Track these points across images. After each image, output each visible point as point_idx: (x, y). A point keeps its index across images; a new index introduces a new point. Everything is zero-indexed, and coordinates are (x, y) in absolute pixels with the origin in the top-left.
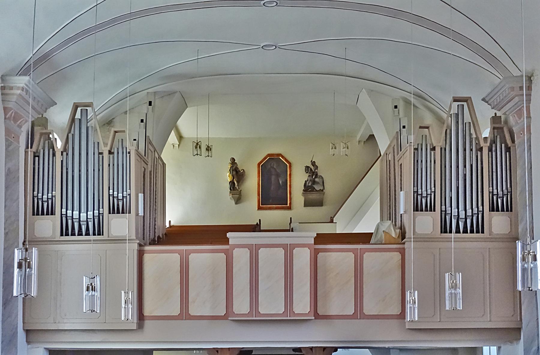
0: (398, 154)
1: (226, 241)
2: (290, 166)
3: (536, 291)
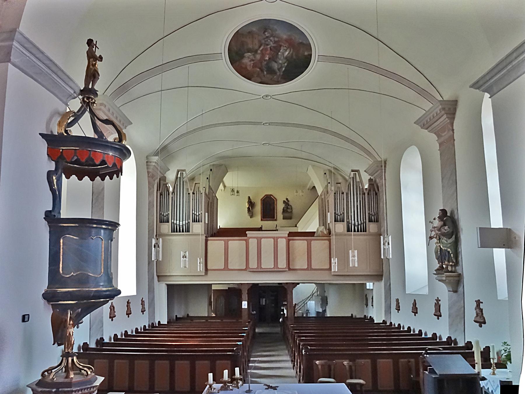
0: (326, 195)
1: (246, 235)
2: (276, 200)
3: (389, 259)
